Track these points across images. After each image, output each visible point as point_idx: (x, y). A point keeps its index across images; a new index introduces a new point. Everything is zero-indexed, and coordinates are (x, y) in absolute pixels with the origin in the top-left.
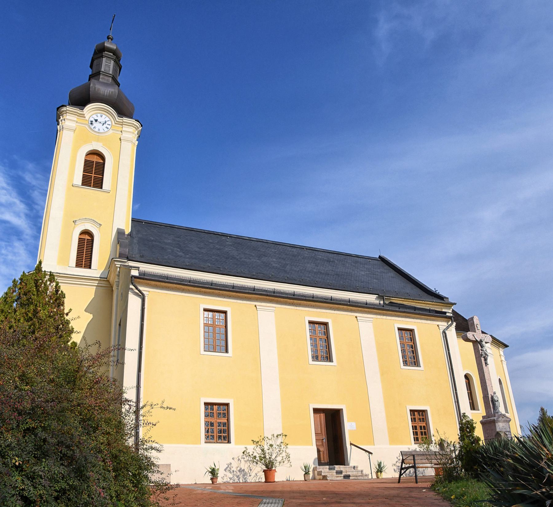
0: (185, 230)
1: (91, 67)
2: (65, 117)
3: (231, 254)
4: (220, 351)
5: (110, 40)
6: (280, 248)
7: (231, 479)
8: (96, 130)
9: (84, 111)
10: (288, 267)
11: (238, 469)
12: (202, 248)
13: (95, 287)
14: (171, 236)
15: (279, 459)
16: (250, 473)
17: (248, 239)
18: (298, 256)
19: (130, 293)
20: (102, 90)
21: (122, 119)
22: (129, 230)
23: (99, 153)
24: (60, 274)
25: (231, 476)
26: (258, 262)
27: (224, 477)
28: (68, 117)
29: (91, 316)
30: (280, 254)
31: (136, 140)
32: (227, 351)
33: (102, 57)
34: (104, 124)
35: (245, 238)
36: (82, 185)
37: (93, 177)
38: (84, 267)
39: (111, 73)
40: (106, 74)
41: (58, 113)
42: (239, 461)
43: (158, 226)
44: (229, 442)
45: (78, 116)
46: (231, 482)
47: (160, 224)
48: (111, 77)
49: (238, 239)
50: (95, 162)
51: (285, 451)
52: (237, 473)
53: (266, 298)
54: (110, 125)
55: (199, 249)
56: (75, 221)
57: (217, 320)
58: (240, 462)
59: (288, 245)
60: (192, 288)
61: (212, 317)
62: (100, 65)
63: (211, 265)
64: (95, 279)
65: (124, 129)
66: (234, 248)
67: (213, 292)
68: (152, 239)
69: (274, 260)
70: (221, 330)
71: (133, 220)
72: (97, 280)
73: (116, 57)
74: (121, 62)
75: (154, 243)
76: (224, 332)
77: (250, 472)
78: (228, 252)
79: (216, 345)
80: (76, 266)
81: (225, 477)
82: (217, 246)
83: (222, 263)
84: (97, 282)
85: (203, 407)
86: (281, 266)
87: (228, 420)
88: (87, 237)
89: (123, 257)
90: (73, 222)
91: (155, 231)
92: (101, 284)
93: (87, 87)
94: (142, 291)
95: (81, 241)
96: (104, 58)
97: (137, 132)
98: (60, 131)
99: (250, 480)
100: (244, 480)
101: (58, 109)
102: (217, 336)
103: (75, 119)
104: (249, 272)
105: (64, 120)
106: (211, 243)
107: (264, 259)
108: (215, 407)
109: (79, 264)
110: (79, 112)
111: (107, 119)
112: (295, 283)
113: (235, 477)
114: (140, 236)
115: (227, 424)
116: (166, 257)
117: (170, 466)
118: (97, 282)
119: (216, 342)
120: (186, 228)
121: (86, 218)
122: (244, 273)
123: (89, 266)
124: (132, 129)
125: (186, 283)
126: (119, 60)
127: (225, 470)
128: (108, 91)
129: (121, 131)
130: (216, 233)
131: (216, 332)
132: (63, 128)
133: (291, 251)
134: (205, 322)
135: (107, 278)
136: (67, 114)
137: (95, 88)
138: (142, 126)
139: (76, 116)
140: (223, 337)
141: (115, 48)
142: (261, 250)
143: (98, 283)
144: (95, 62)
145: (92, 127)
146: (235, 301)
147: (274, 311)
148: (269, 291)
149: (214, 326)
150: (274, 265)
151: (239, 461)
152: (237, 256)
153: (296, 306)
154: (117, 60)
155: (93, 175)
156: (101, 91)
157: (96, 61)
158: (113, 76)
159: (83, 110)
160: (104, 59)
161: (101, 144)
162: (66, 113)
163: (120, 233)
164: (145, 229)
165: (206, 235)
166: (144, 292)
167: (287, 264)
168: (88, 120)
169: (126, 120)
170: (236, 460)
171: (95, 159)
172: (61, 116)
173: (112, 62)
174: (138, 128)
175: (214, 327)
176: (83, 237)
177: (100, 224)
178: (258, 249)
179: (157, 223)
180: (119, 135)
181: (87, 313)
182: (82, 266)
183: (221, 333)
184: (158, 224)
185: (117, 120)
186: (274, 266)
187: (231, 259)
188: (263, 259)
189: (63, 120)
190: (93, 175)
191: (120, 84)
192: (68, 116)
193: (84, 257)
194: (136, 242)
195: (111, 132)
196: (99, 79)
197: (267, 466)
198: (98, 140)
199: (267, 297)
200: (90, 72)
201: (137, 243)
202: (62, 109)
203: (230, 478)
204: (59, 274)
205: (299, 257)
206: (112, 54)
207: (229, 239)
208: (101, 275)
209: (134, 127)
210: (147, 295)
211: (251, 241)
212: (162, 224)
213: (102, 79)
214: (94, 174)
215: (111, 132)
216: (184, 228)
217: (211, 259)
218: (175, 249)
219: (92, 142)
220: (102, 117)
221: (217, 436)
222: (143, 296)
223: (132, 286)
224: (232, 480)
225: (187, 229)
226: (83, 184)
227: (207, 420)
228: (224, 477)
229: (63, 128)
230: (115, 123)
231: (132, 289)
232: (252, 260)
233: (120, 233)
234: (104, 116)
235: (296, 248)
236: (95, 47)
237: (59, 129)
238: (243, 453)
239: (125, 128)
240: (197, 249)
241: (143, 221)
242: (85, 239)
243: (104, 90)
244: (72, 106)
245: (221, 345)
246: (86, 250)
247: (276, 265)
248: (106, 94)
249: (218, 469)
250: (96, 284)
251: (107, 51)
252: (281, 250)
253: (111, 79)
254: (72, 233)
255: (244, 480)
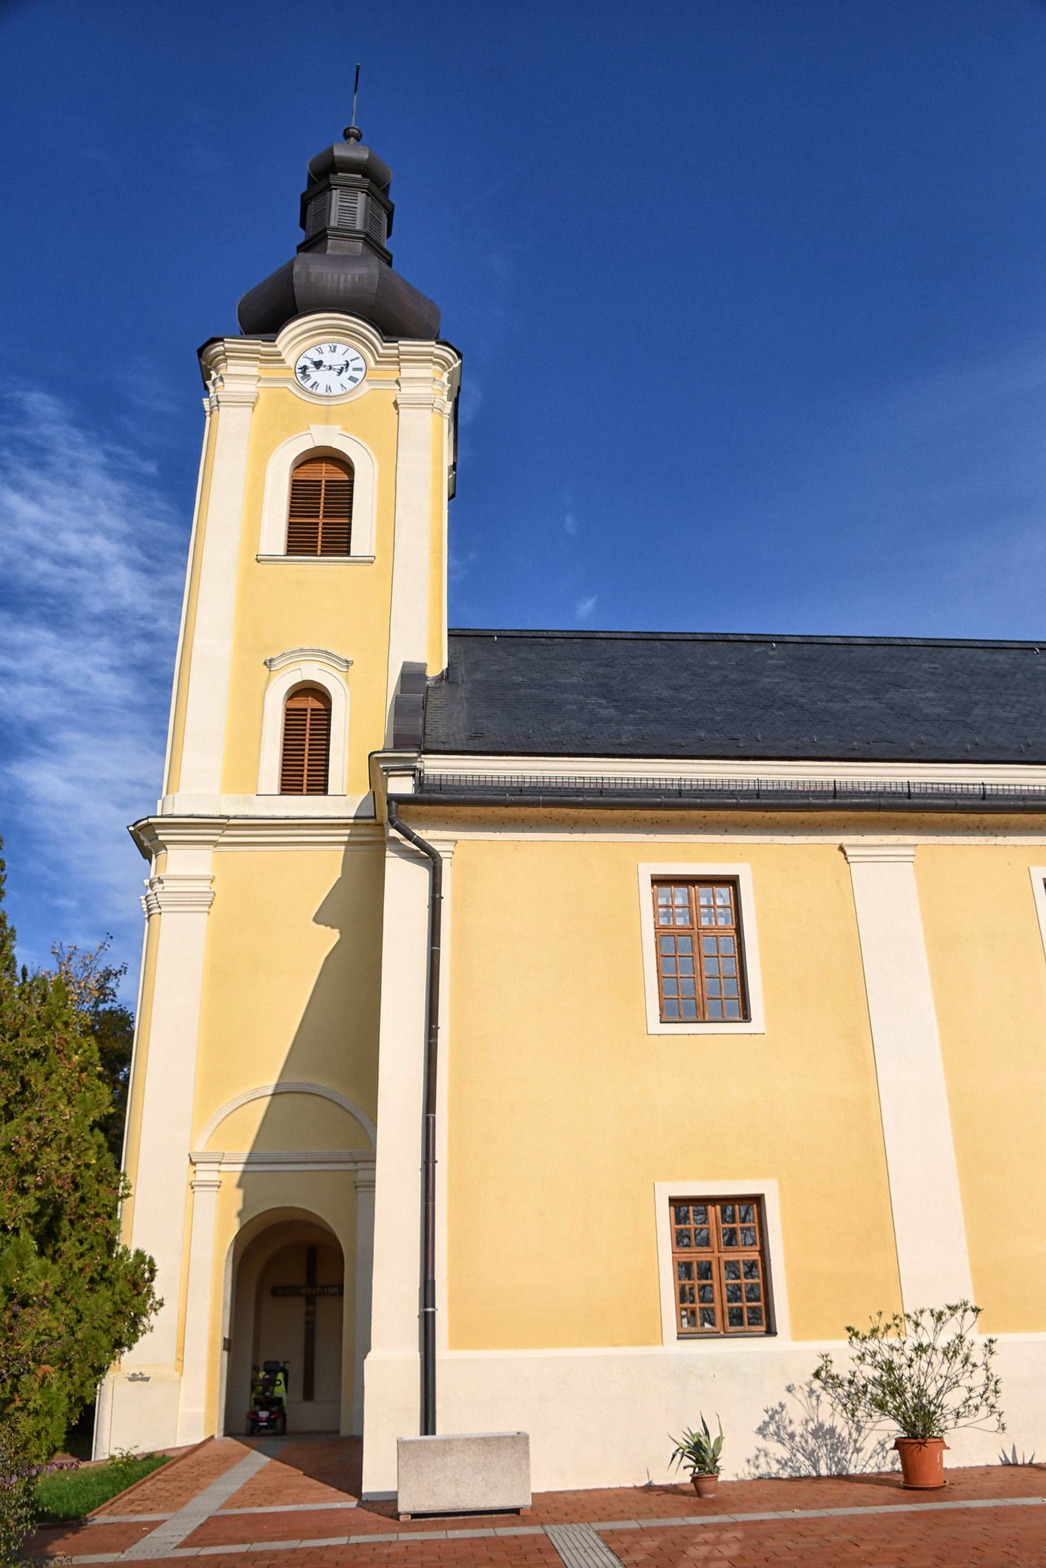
0: (630, 643)
1: (303, 225)
2: (222, 372)
3: (781, 693)
4: (721, 1018)
5: (352, 139)
6: (951, 656)
7: (783, 1464)
8: (321, 390)
9: (276, 343)
10: (976, 711)
11: (811, 1426)
12: (682, 687)
13: (343, 848)
14: (583, 663)
15: (953, 1400)
16: (856, 1441)
17: (840, 641)
18: (1014, 674)
19: (388, 853)
20: (330, 278)
21: (396, 344)
22: (441, 665)
23: (334, 455)
24: (228, 818)
25: (782, 1452)
26: (873, 708)
27: (757, 1457)
28: (231, 370)
29: (334, 935)
30: (951, 674)
31: (445, 398)
32: (746, 1017)
33: (329, 188)
34: (341, 370)
35: (829, 640)
36: (287, 555)
37: (321, 525)
38: (308, 790)
39: (359, 226)
40: (345, 233)
41: (204, 363)
42: (814, 1398)
43: (543, 640)
44: (771, 1331)
45: (261, 361)
46: (785, 1477)
47: (550, 634)
48: (360, 238)
49: (806, 647)
50: (323, 482)
51: (986, 1364)
52: (806, 1442)
53: (878, 819)
54: (360, 369)
55: (671, 692)
56: (271, 661)
57: (704, 910)
58: (814, 1402)
59: (979, 644)
60: (607, 813)
61: (687, 904)
62: (325, 212)
63: (708, 735)
64: (339, 825)
65: (405, 373)
66: (792, 676)
67: (682, 819)
68: (520, 679)
69: (931, 694)
70: (721, 945)
71: (452, 635)
72: (347, 824)
73: (371, 180)
74: (391, 197)
75: (522, 691)
76: (732, 950)
77: (855, 1435)
78: (769, 690)
79: (706, 995)
80: (283, 790)
81: (762, 1460)
82: (733, 676)
83: (747, 723)
84: (348, 832)
85: (664, 1214)
86: (951, 710)
87: (764, 1252)
88: (312, 703)
89: (407, 746)
90: (265, 663)
91: (532, 656)
92: (360, 835)
93: (286, 275)
94: (430, 843)
95: (293, 719)
96: (334, 191)
97: (446, 375)
98: (211, 413)
99: (859, 1468)
100: (834, 1469)
101: (200, 352)
102: (709, 967)
103: (254, 371)
104: (841, 741)
105: (222, 379)
106: (713, 668)
107: (894, 696)
108: (713, 1211)
109: (289, 786)
110: (262, 349)
111: (352, 354)
112: (1002, 758)
113: (799, 1456)
114: (479, 676)
115: (761, 1267)
116: (557, 729)
117: (527, 1444)
118: (348, 832)
119: (705, 987)
120: (634, 636)
121: (302, 650)
122: (823, 747)
123: (320, 787)
124: (429, 370)
125: (581, 799)
126: (386, 191)
127: (761, 1431)
128: (349, 277)
129: (397, 382)
130: (732, 638)
131: (704, 952)
132: (218, 402)
133: (988, 661)
134: (663, 922)
135: (375, 817)
136: (228, 361)
137: (309, 274)
138: (460, 356)
139: (258, 363)
140: (732, 967)
141: (366, 156)
142: (887, 669)
143: (349, 835)
144: (312, 207)
145: (308, 385)
146: (766, 839)
147: (911, 859)
148: (888, 793)
149: (693, 932)
150: (928, 710)
151: (814, 1398)
152: (802, 696)
153: (991, 834)
154: (374, 189)
155: (321, 521)
156: (327, 279)
157: (313, 203)
158: (367, 234)
159: (274, 341)
160: (336, 194)
161: (337, 428)
162: (225, 360)
163: (412, 676)
164: (500, 653)
165: (701, 648)
166: (437, 847)
167: (976, 704)
168: (293, 367)
169: (406, 345)
170: (801, 1395)
171: (325, 473)
172: (212, 372)
173: (361, 197)
174: (449, 364)
175: (695, 938)
176: (298, 703)
177: (347, 661)
178: (876, 669)
179: (540, 634)
180: (391, 393)
181: (323, 927)
182: (301, 790)
183: (722, 953)
184: (545, 634)
185: (381, 351)
186: (927, 715)
187: (780, 709)
188: (889, 695)
189: (218, 380)
190: (321, 521)
191: (391, 257)
192: (231, 368)
193: (306, 762)
194: (463, 695)
195: (366, 388)
196: (326, 251)
197: (908, 1426)
198: (327, 419)
199: (882, 814)
200: (301, 236)
201: (467, 699)
202: (214, 351)
203: (778, 1462)
204: (225, 821)
205: (1019, 676)
206: (360, 176)
207: (775, 650)
208: (357, 812)
209: (435, 363)
210: (450, 855)
211: (852, 648)
212: (556, 634)
213: (331, 249)
214: (324, 516)
215: (366, 388)
216: (629, 636)
217: (710, 715)
218: (593, 700)
219: (309, 429)
220: (334, 351)
221: (726, 1310)
222: (433, 858)
223: (393, 833)
224: (789, 1470)
225: (638, 636)
226: (290, 552)
227: (684, 1258)
228: (757, 1457)
229: (218, 402)
230: (377, 362)
231: (395, 839)
232: (853, 703)
233: (412, 676)
234: (341, 348)
235: (1007, 651)
236: (308, 167)
237: (207, 408)
238: (817, 1375)
239: (408, 371)
240: (666, 693)
241: (493, 633)
242: (306, 710)
243: (336, 276)
244: (248, 336)
245: (724, 996)
246: (310, 740)
247: (937, 710)
248: (342, 286)
249: (719, 1440)
250: (345, 839)
251: (341, 172)
252: (955, 662)
253: (361, 244)
254: (264, 698)
255: (834, 1469)
